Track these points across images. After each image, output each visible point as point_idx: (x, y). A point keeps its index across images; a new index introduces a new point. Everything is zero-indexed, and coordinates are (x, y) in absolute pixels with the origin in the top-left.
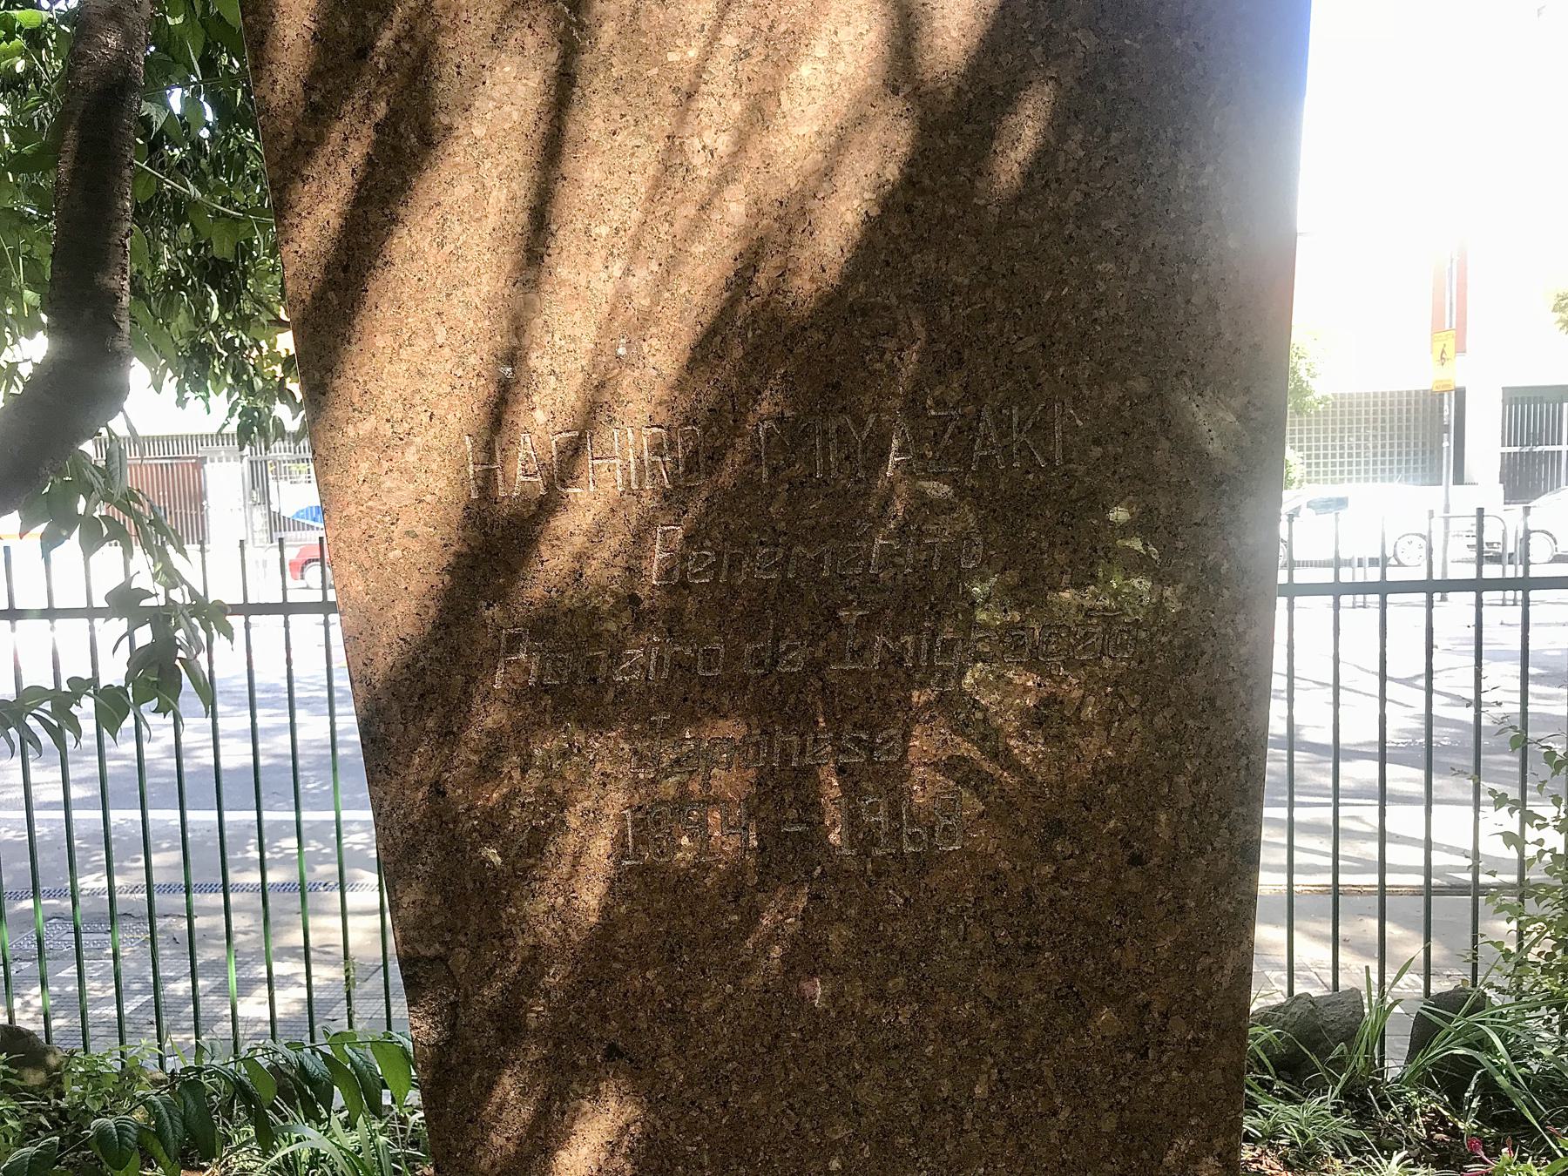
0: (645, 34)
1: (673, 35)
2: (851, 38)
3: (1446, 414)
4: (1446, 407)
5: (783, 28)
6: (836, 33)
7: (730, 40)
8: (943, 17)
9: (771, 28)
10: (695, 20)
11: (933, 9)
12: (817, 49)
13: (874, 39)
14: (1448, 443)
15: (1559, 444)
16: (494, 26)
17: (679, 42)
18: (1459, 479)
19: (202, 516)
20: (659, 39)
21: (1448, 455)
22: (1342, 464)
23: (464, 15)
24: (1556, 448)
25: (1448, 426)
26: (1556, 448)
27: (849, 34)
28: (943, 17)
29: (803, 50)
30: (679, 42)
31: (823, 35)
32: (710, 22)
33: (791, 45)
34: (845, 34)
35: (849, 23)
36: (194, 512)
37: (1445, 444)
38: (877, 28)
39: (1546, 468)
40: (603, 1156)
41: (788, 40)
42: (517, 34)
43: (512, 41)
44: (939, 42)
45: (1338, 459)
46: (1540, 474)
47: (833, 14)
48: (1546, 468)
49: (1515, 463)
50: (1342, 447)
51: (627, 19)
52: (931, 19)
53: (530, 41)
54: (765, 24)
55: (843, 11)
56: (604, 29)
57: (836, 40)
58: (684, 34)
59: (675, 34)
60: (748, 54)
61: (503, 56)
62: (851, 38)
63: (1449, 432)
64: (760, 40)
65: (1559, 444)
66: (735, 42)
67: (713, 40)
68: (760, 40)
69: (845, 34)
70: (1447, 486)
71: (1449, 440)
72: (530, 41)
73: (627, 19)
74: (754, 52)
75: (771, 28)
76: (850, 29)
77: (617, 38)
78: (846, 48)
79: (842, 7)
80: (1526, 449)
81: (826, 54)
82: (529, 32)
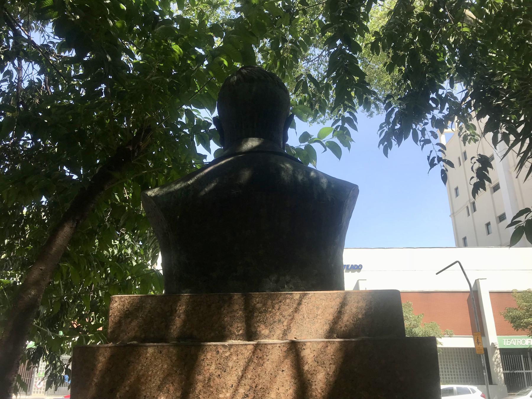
0: (212, 387)
1: (222, 388)
2: (284, 391)
3: (483, 362)
4: (482, 360)
5: (260, 387)
6: (278, 389)
7: (242, 391)
8: (315, 385)
9: (256, 387)
10: (230, 383)
11: (312, 382)
12: (272, 395)
13: (292, 392)
14: (485, 374)
15: (522, 370)
16: (159, 382)
17: (224, 390)
18: (491, 382)
19: (31, 380)
20: (217, 389)
21: (486, 377)
22: (449, 375)
23: (149, 378)
24: (521, 371)
25: (484, 367)
26: (521, 371)
27: (283, 390)
28: (315, 385)
29: (267, 395)
30: (224, 390)
31: (274, 390)
32: (235, 384)
33: (263, 393)
34: (282, 390)
35: (283, 386)
36: (26, 378)
37: (485, 374)
38: (293, 388)
39: (520, 379)
40: (211, 61)
41: (262, 391)
42: (167, 386)
43: (165, 388)
44: (314, 394)
45: (447, 373)
46: (518, 381)
47: (278, 382)
48: (520, 379)
49: (509, 376)
50: (448, 368)
51: (206, 382)
52: (311, 385)
53: (172, 388)
54: (254, 385)
55: (281, 382)
56: (198, 385)
57: (278, 392)
58: (226, 388)
59: (223, 388)
60: (247, 396)
61: (161, 393)
62: (284, 391)
63: (485, 369)
64: (252, 391)
65: (522, 370)
66: (243, 391)
67: (236, 390)
68: (252, 391)
69: (282, 390)
70: (487, 384)
71: (486, 373)
72: (172, 388)
73: (206, 382)
74: (249, 395)
75: (256, 387)
76: (283, 388)
77: (202, 388)
78: (282, 395)
79: (281, 380)
80: (511, 372)
81: (275, 397)
82: (171, 385)
